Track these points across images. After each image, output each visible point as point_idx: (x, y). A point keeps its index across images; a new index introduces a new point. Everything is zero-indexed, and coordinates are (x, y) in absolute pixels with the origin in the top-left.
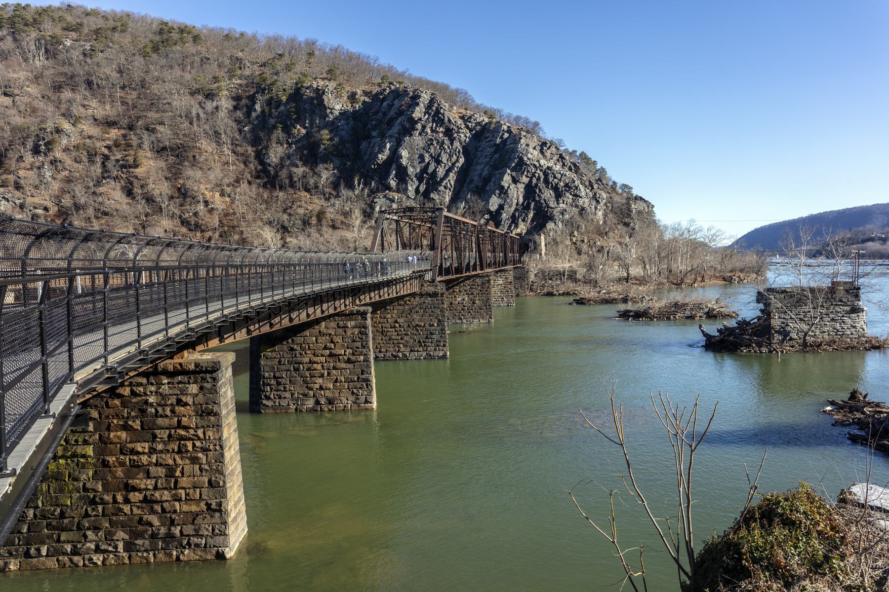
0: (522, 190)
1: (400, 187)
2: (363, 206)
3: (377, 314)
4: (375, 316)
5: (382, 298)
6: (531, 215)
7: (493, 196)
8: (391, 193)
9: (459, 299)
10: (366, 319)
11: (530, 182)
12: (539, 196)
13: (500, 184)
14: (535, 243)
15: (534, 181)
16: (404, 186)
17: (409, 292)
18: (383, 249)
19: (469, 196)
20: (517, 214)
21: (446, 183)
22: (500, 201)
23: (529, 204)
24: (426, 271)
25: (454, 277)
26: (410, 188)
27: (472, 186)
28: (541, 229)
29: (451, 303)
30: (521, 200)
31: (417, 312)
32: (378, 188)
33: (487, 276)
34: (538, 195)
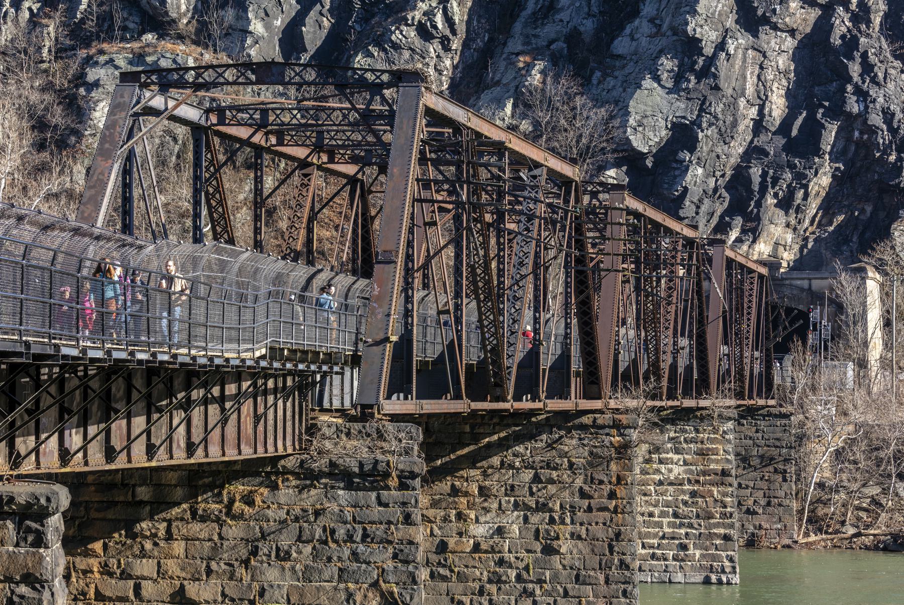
0: (783, 62)
1: (213, 16)
2: (35, 97)
3: (87, 554)
4: (81, 563)
5: (120, 463)
6: (822, 181)
7: (648, 83)
8: (167, 45)
9: (479, 531)
10: (40, 541)
11: (823, 26)
12: (861, 94)
13: (679, 31)
14: (839, 308)
15: (842, 23)
16: (229, 14)
17: (247, 452)
18: (127, 228)
19: (535, 78)
20: (756, 172)
21: (429, 14)
22: (681, 108)
23: (813, 130)
24: (330, 359)
25: (462, 406)
26: (257, 27)
27: (549, 30)
28: (866, 247)
29: (442, 547)
30: (778, 106)
31: (283, 556)
32: (105, 19)
33: (617, 426)
34: (861, 94)
